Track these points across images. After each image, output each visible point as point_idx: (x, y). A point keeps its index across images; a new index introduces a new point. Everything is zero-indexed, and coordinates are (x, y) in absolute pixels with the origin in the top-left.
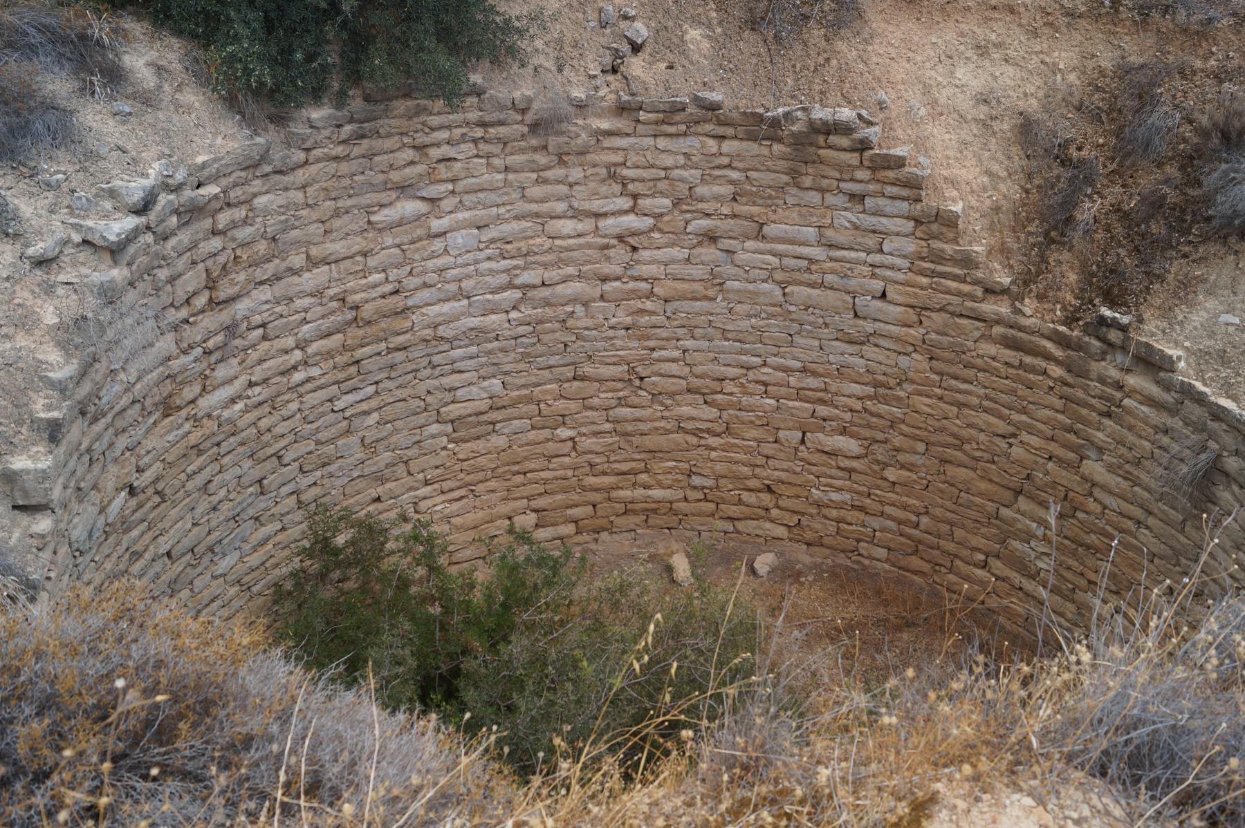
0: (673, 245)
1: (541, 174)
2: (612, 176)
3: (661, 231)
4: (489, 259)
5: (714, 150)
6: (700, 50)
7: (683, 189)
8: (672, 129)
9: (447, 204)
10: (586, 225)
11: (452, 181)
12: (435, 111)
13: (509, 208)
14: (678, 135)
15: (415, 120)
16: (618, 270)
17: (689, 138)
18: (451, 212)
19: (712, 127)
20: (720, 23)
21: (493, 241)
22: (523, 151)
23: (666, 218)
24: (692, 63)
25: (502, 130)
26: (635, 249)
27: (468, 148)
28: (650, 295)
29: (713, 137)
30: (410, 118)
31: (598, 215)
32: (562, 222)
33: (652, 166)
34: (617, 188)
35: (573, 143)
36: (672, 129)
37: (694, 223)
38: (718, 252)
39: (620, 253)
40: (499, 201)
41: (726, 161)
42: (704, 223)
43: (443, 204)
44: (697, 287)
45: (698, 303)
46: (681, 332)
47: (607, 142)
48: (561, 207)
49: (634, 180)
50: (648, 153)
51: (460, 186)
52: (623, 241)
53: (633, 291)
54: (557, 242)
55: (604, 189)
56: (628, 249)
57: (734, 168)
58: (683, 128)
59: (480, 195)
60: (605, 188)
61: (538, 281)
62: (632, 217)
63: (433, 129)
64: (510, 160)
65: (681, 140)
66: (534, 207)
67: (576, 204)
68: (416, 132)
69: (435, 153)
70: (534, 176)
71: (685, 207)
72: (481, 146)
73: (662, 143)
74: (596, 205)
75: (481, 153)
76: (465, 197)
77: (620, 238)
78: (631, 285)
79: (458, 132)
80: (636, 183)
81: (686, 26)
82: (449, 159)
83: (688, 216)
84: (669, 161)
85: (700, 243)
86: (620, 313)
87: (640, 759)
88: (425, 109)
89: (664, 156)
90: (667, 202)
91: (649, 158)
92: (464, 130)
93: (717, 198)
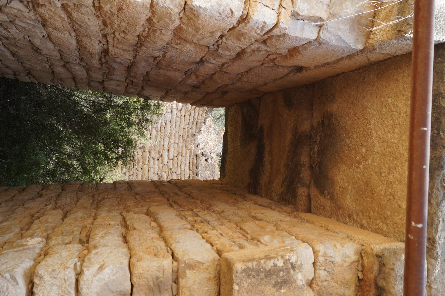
0: (159, 169)
2: (179, 153)
3: (163, 166)
4: (162, 123)
7: (174, 170)
8: (191, 166)
9: (179, 114)
10: (166, 147)
16: (152, 156)
21: (166, 123)
22: (188, 132)
23: (167, 167)
25: (194, 128)
26: (158, 160)
27: (192, 119)
28: (144, 164)
31: (168, 150)
33: (181, 163)
36: (191, 166)
39: (157, 156)
43: (179, 113)
46: (132, 172)
47: (188, 152)
51: (183, 117)
53: (146, 159)
55: (176, 152)
61: (152, 135)
62: (167, 159)
63: (198, 112)
65: (188, 169)
67: (172, 145)
72: (192, 123)
73: (188, 165)
74: (171, 150)
77: (161, 156)
78: (148, 159)
82: (190, 115)
83: (167, 172)
84: (183, 166)
86: (139, 156)
87: (401, 18)
88: (204, 111)
90: (171, 167)
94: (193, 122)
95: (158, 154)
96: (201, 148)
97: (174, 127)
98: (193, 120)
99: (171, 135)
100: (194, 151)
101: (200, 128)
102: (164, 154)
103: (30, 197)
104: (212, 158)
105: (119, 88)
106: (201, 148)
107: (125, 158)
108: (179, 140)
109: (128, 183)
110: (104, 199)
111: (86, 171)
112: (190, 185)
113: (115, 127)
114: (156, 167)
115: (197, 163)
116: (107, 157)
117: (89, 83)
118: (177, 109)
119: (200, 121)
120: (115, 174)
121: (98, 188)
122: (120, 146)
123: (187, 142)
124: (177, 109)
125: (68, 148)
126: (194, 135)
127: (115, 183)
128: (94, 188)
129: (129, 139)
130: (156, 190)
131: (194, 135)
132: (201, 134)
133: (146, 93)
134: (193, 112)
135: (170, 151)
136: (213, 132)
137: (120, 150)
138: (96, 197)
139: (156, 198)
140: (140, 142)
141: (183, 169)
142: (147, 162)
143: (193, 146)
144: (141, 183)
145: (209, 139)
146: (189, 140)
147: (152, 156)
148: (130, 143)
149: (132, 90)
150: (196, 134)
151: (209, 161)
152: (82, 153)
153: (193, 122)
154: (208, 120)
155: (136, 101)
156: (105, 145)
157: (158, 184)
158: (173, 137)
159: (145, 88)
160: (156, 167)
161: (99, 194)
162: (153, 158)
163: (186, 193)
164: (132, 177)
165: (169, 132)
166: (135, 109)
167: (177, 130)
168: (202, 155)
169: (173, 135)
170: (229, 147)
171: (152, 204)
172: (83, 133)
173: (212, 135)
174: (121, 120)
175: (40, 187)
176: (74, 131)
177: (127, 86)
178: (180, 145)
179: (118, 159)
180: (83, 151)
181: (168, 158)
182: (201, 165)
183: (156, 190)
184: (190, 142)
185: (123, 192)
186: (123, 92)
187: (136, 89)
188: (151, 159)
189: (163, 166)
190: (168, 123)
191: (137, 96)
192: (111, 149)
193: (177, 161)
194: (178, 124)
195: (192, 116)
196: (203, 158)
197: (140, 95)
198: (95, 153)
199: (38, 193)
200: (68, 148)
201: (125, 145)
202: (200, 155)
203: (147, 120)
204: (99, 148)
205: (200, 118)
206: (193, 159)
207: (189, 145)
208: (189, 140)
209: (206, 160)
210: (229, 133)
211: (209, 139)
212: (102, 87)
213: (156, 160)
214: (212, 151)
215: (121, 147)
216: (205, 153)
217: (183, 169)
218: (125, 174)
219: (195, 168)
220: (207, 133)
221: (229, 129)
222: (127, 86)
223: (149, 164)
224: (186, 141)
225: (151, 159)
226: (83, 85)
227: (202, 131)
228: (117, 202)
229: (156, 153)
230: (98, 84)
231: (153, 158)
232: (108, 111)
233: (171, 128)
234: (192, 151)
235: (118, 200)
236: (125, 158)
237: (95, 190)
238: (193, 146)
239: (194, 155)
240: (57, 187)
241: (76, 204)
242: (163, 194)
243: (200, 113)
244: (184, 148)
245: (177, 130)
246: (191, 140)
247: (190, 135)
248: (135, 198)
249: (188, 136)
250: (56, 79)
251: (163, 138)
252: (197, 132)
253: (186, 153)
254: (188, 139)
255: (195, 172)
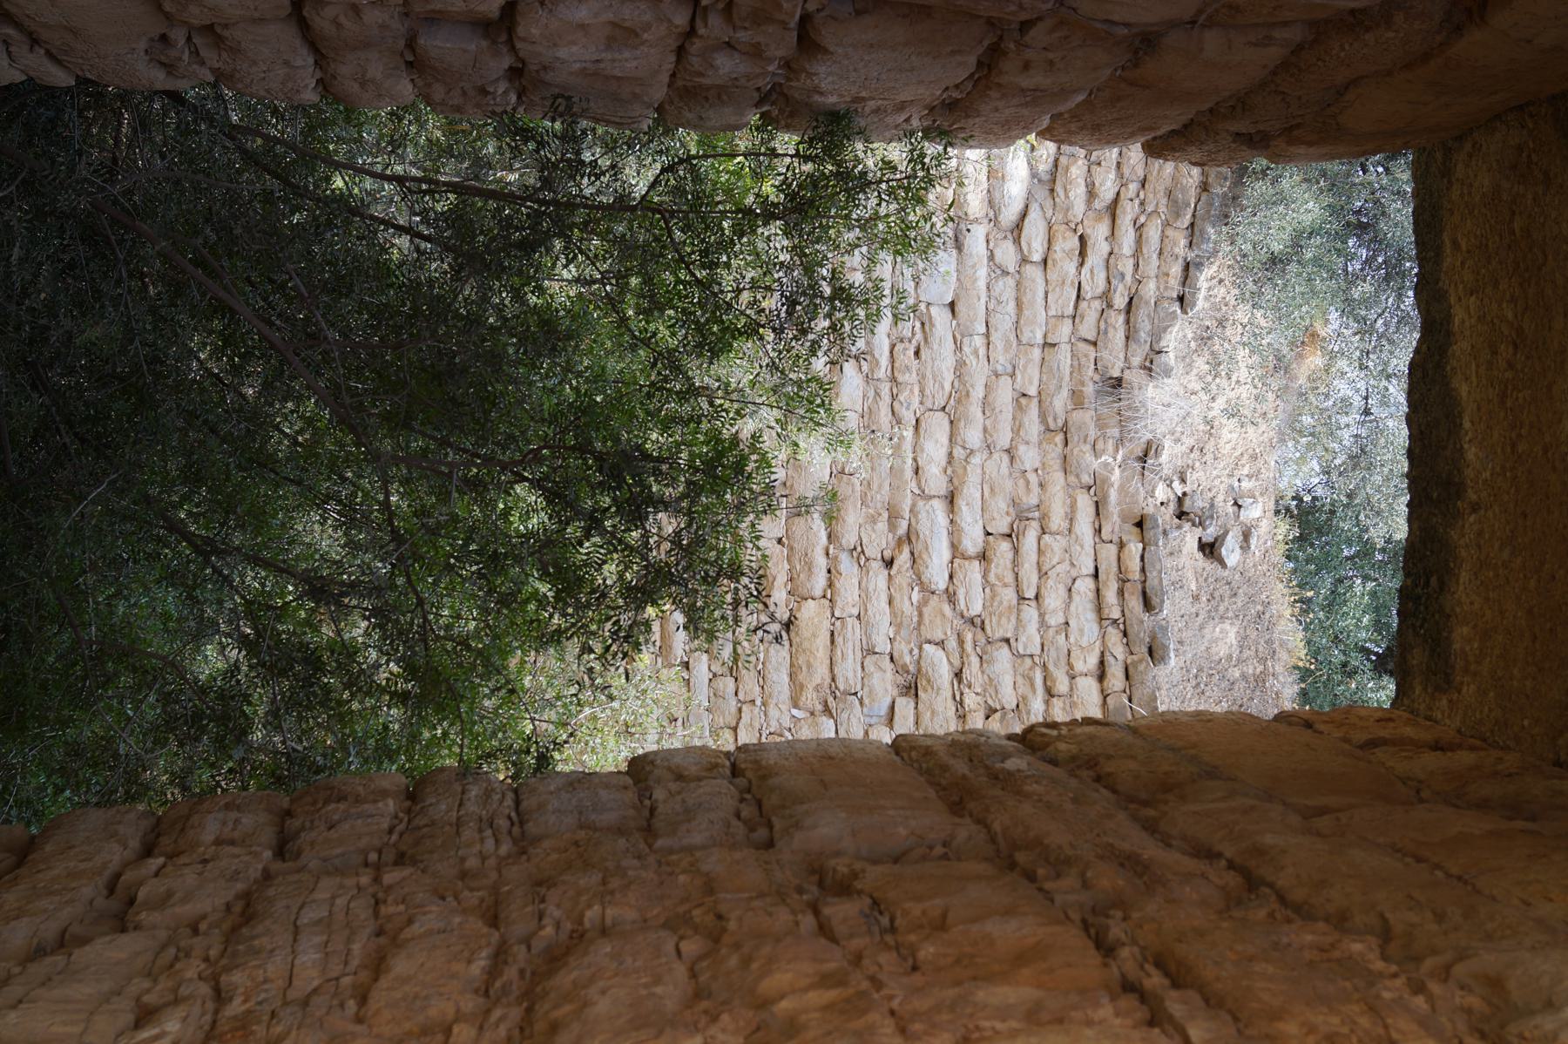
0: (897, 623)
1: (1036, 401)
2: (1022, 516)
3: (924, 603)
5: (1079, 666)
6: (1216, 641)
7: (998, 629)
8: (1110, 596)
9: (1007, 254)
10: (936, 481)
11: (1045, 261)
12: (1170, 232)
13: (982, 352)
14: (1099, 609)
15: (1164, 201)
16: (850, 539)
17: (1095, 627)
18: (991, 257)
19: (1120, 657)
20: (1244, 677)
22: (1077, 368)
23: (947, 609)
24: (1201, 628)
25: (1118, 336)
26: (889, 563)
27: (1095, 282)
28: (798, 595)
29: (1102, 663)
30: (1169, 194)
31: (951, 499)
32: (945, 440)
33: (1043, 575)
34: (1002, 525)
35: (1087, 448)
36: (1110, 596)
37: (941, 653)
38: (888, 700)
39: (879, 540)
40: (995, 337)
41: (1062, 685)
42: (944, 673)
44: (821, 673)
45: (786, 679)
47: (1085, 503)
48: (973, 436)
49: (1016, 550)
50: (1066, 566)
51: (1034, 273)
52: (900, 543)
53: (810, 566)
54: (909, 434)
55: (1000, 504)
56: (888, 554)
57: (1047, 703)
58: (1116, 614)
59: (1011, 307)
60: (1003, 505)
62: (946, 555)
63: (1139, 228)
64: (1063, 357)
65: (1091, 616)
66: (978, 393)
67: (976, 460)
68: (1142, 203)
69: (1098, 233)
70: (1033, 391)
71: (969, 637)
73: (1085, 586)
74: (971, 493)
75: (1083, 305)
76: (1010, 281)
77: (909, 538)
78: (821, 562)
79: (1127, 266)
80: (1010, 555)
81: (1238, 623)
82: (1083, 254)
83: (952, 644)
84: (1054, 600)
85: (900, 669)
88: (1178, 215)
89: (1062, 591)
90: (976, 608)
91: (1059, 568)
92: (1128, 278)
93: (992, 684)
94: (1106, 297)
95: (882, 526)
96: (1166, 471)
97: (979, 341)
98: (1101, 284)
99: (961, 394)
100: (1122, 489)
101: (1157, 334)
102: (923, 527)
103: (50, 930)
104: (1246, 536)
105: (628, 62)
106: (1166, 471)
107: (704, 581)
108: (1017, 430)
109: (735, 771)
110: (579, 938)
111: (436, 686)
112: (1212, 773)
113: (613, 365)
114: (879, 609)
115: (1152, 575)
116: (571, 583)
117: (411, 44)
118: (994, 221)
119: (1150, 289)
120: (644, 705)
121: (531, 827)
122: (662, 504)
123: (1074, 438)
124: (994, 221)
125: (320, 536)
126: (1118, 383)
127: (639, 767)
128: (503, 823)
129: (714, 437)
130: (962, 834)
131: (1118, 383)
132: (1167, 372)
133: (830, 83)
134: (1103, 229)
135: (961, 503)
136: (1242, 353)
137: (667, 523)
138: (519, 919)
139: (993, 927)
140: (808, 461)
141: (1055, 620)
142: (819, 583)
143: (1111, 464)
144: (834, 768)
145: (1221, 403)
146: (1085, 418)
147: (850, 539)
148: (726, 472)
149: (727, 66)
150: (1134, 377)
151: (1231, 552)
152: (400, 565)
153: (1106, 297)
154: (1203, 279)
155: (761, 161)
156: (557, 497)
157: (960, 767)
158: (975, 410)
159: (828, 35)
160: (879, 609)
161: (541, 884)
162: (857, 552)
163: (1211, 855)
164: (730, 682)
165: (948, 377)
166: (748, 220)
167: (1002, 360)
168: (1181, 515)
169: (978, 393)
170: (1471, 453)
171: (981, 995)
172: (399, 422)
173: (1242, 373)
174: (653, 305)
175: (131, 824)
176: (349, 418)
177: (691, 32)
178: (1029, 456)
179: (641, 594)
180: (405, 546)
181: (954, 547)
182: (1179, 584)
183: (966, 831)
184: (1093, 433)
185: (714, 863)
186: (659, 93)
187: (756, 53)
188: (846, 564)
189: (924, 603)
190: (940, 316)
191: (755, 119)
192: (593, 523)
193: (1016, 563)
194: (1004, 322)
195: (1096, 258)
196: (1189, 538)
197: (780, 107)
198: (497, 556)
199: (111, 889)
200: (320, 536)
201: (693, 490)
202: (1166, 516)
203: (843, 295)
204: (514, 518)
205: (1152, 264)
206: (1122, 545)
207: (1089, 457)
208: (1086, 417)
209: (1209, 549)
210: (1460, 348)
211: (1221, 403)
212: (507, 61)
213: (876, 565)
214: (1246, 484)
215: (662, 515)
216: (1197, 504)
217: (1055, 620)
218: (686, 665)
219: (1135, 603)
220: (1201, 364)
221: (1459, 315)
222: (691, 32)
223: (830, 595)
224: (1065, 430)
225: (846, 564)
226: (375, 70)
227: (1170, 358)
228: (681, 971)
229: (873, 520)
230: (475, 44)
231: (857, 552)
232: (558, 244)
233: (958, 347)
234: (1113, 496)
235: (691, 947)
236: (704, 581)
237: (504, 849)
238: (1111, 464)
239: (1124, 519)
240: (248, 821)
241: (363, 1000)
242: (1031, 877)
243: (1153, 233)
244: (1057, 478)
245: (1002, 360)
246: (1101, 424)
247: (1089, 389)
248: (824, 930)
249: (1077, 398)
250: (178, 36)
251: (908, 417)
252: (1136, 360)
253: (1073, 506)
254: (1077, 416)
255: (1141, 635)
